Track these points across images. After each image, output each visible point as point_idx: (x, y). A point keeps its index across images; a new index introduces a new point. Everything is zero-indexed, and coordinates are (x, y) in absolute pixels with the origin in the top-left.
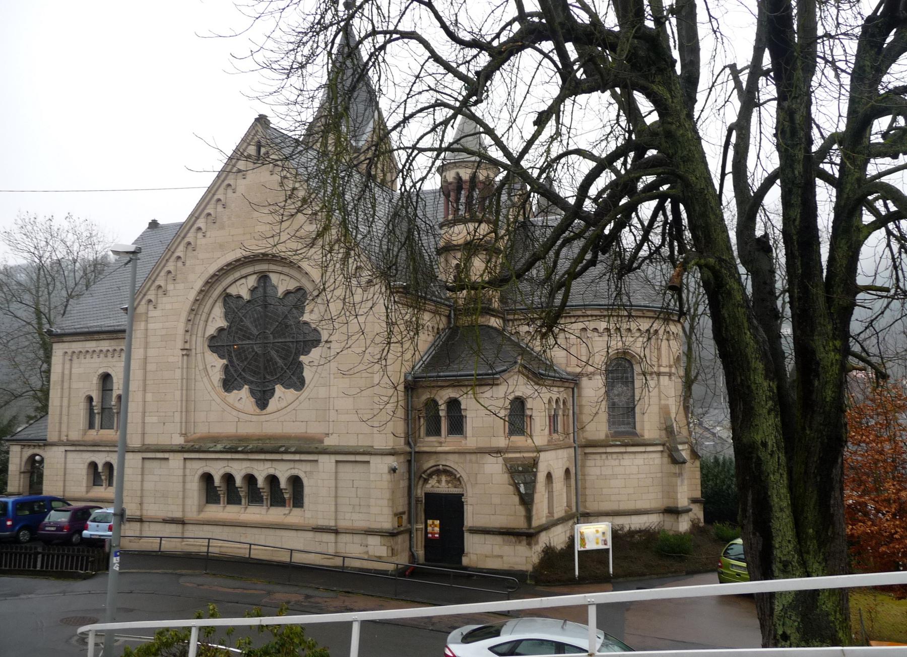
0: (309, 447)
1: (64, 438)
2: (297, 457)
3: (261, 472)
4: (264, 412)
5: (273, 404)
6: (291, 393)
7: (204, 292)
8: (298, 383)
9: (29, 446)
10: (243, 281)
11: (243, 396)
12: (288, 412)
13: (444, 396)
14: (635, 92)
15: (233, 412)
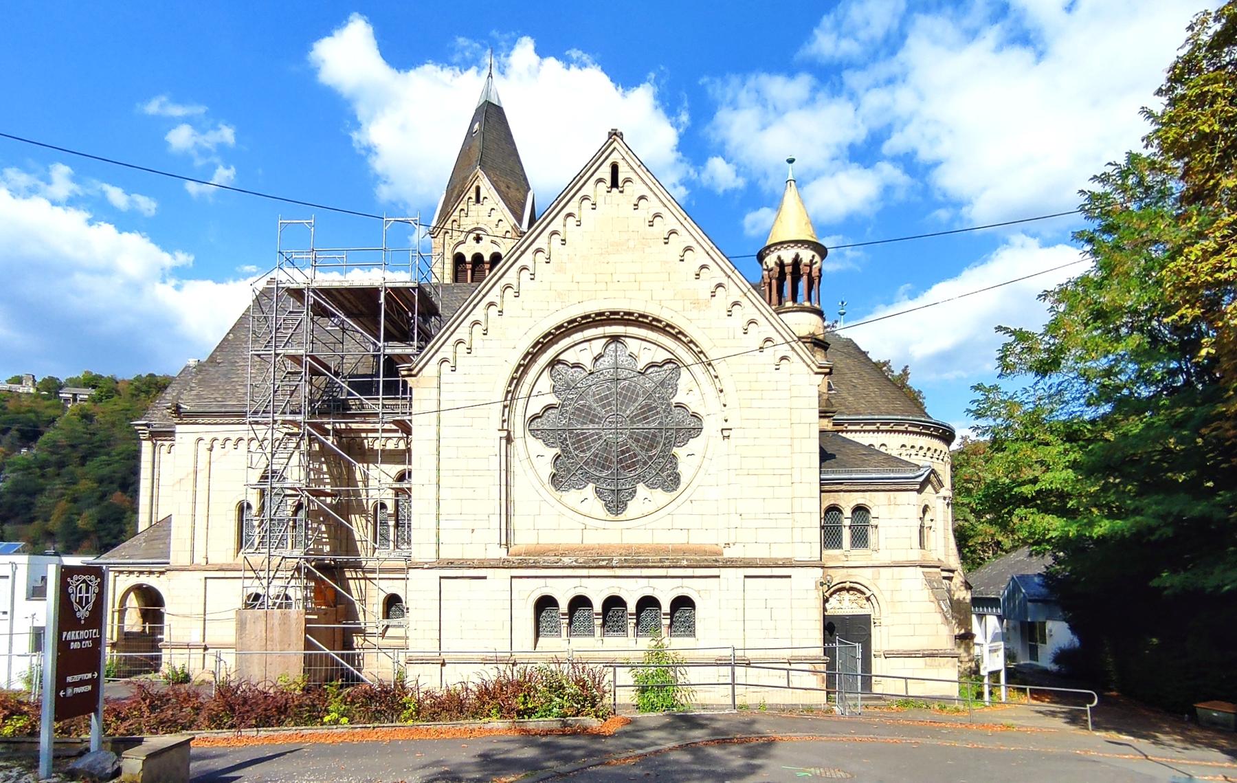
0: (710, 562)
1: (199, 560)
2: (689, 572)
3: (632, 593)
4: (620, 517)
5: (634, 507)
6: (660, 496)
7: (531, 356)
8: (672, 481)
9: (131, 572)
10: (586, 345)
11: (586, 499)
12: (651, 518)
13: (848, 502)
14: (795, 59)
15: (570, 518)
